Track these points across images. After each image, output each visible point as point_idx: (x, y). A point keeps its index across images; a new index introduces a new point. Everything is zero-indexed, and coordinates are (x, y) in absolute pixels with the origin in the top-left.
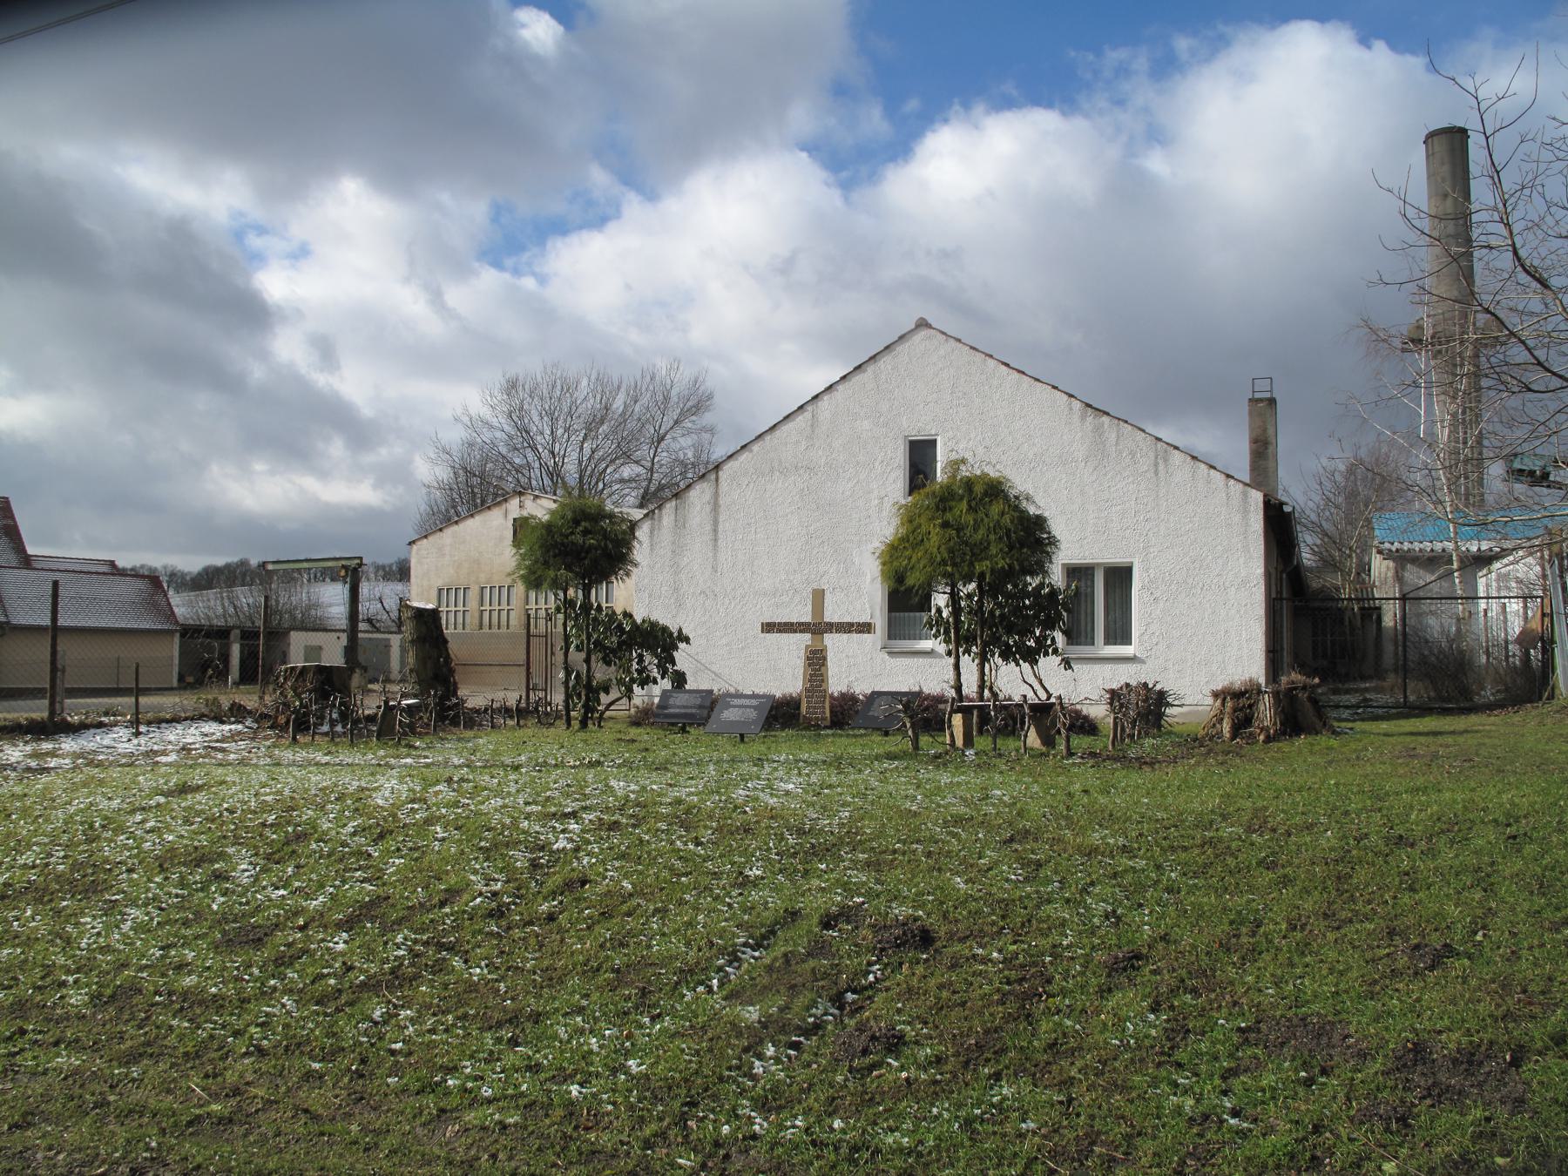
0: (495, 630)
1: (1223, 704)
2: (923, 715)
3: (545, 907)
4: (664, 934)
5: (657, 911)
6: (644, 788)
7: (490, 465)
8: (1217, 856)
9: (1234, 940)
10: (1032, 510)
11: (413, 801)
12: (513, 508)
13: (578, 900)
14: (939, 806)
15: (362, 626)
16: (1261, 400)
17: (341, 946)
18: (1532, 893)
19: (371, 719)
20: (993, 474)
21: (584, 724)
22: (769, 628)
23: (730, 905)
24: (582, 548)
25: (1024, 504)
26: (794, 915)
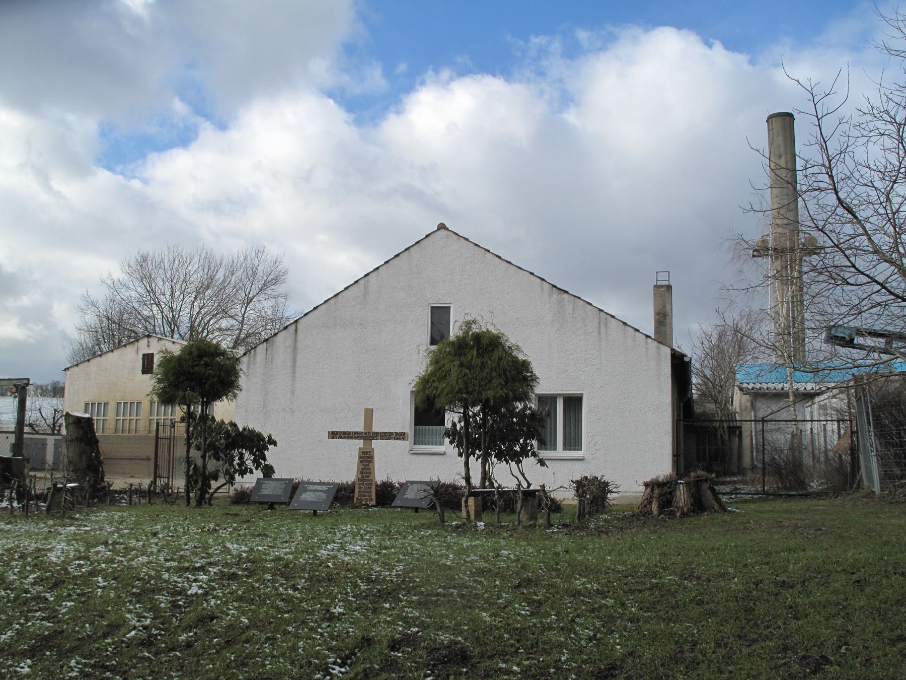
0: (126, 434)
1: (652, 491)
2: (445, 498)
3: (183, 637)
4: (274, 656)
5: (268, 639)
6: (252, 550)
7: (126, 316)
8: (662, 596)
9: (679, 655)
10: (521, 357)
11: (79, 559)
12: (143, 347)
13: (208, 631)
14: (465, 561)
15: (26, 429)
16: (662, 286)
17: (27, 670)
18: (874, 619)
19: (41, 497)
20: (494, 331)
21: (199, 503)
22: (333, 435)
23: (322, 634)
24: (199, 374)
25: (515, 353)
26: (367, 642)
